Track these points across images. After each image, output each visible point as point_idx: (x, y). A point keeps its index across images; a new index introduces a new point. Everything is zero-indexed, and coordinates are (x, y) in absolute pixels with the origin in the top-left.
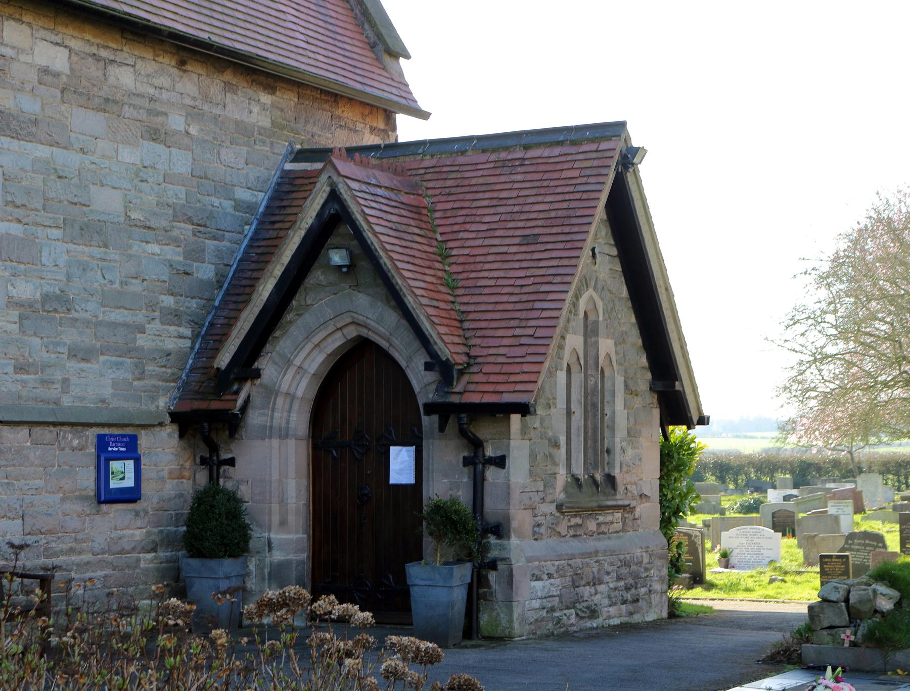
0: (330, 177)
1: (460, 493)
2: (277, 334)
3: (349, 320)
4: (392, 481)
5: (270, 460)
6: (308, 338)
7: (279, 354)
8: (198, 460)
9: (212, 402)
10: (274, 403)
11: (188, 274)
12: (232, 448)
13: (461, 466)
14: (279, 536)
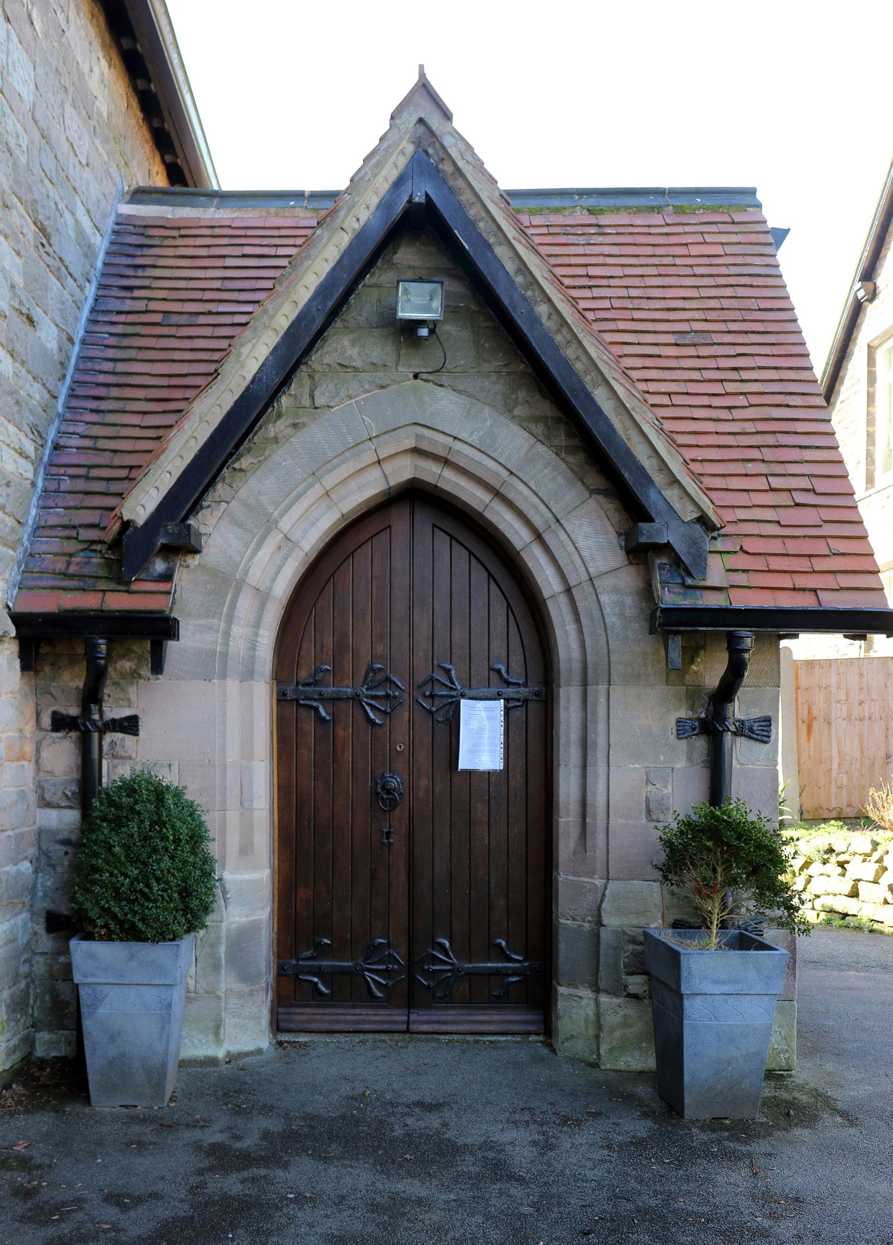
0: (421, 121)
1: (668, 791)
2: (244, 462)
3: (410, 443)
4: (461, 766)
5: (224, 723)
6: (314, 476)
7: (245, 504)
8: (47, 721)
9: (108, 595)
10: (233, 606)
11: (31, 321)
12: (133, 696)
13: (673, 737)
14: (238, 877)
